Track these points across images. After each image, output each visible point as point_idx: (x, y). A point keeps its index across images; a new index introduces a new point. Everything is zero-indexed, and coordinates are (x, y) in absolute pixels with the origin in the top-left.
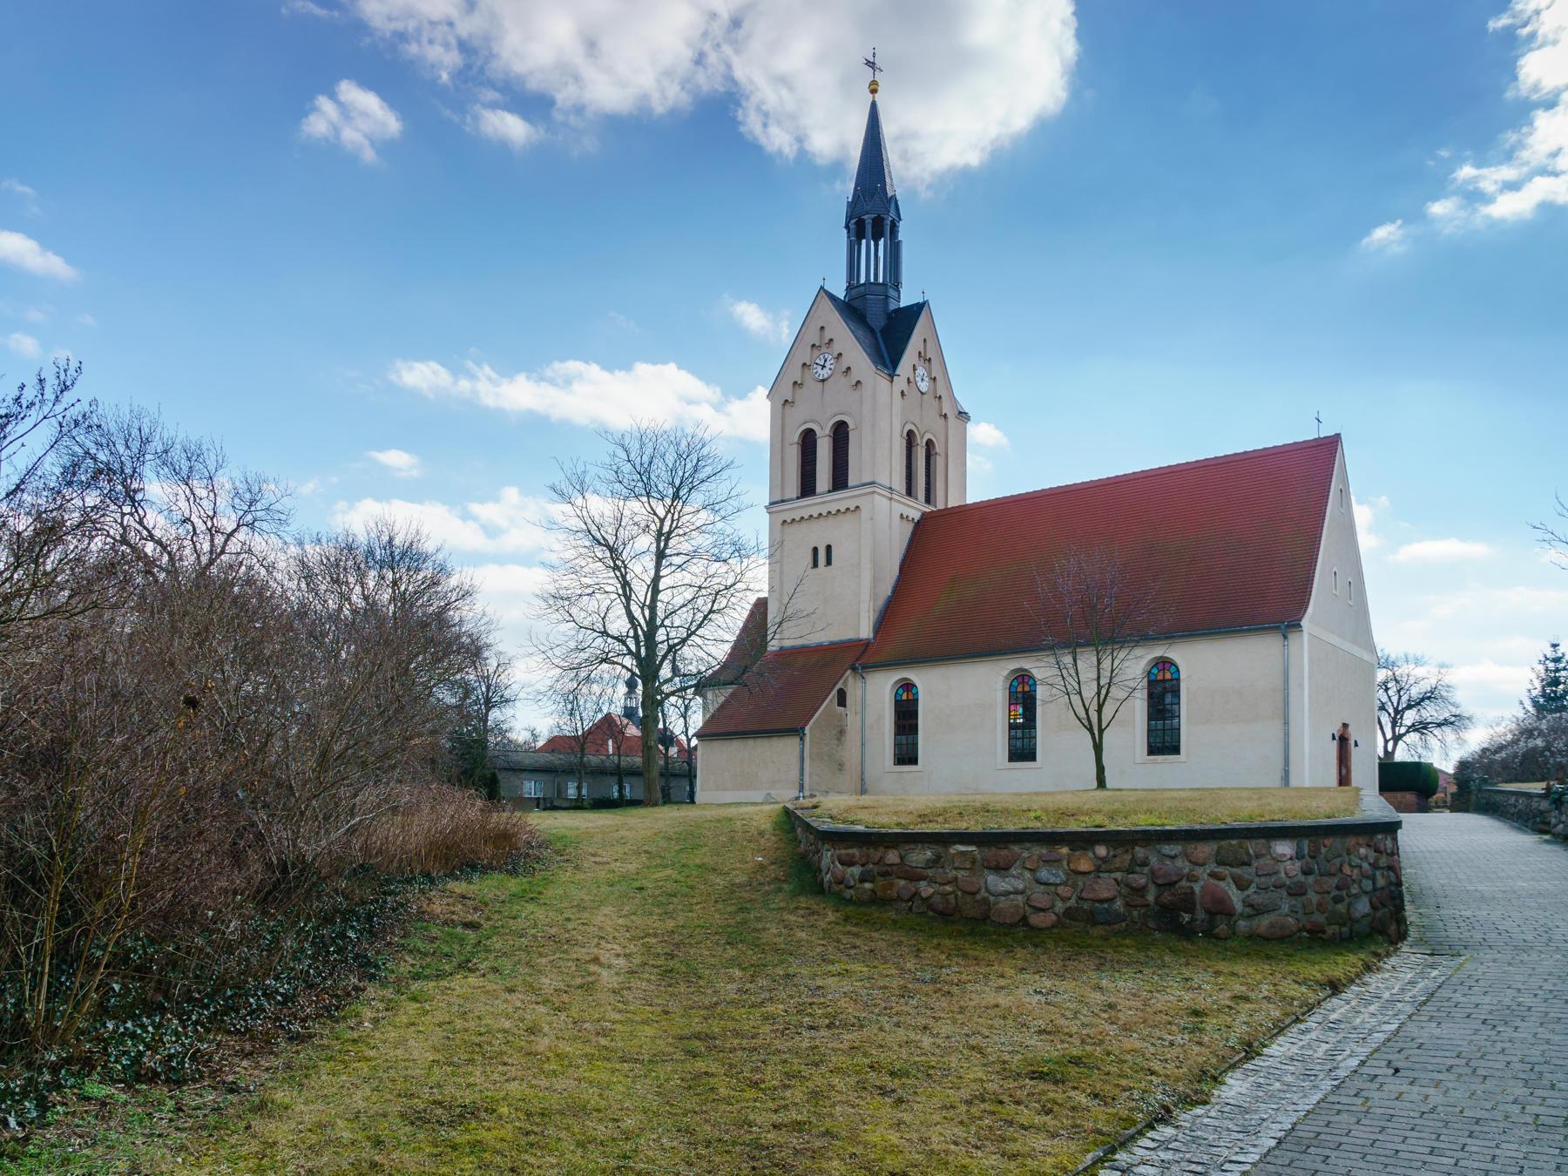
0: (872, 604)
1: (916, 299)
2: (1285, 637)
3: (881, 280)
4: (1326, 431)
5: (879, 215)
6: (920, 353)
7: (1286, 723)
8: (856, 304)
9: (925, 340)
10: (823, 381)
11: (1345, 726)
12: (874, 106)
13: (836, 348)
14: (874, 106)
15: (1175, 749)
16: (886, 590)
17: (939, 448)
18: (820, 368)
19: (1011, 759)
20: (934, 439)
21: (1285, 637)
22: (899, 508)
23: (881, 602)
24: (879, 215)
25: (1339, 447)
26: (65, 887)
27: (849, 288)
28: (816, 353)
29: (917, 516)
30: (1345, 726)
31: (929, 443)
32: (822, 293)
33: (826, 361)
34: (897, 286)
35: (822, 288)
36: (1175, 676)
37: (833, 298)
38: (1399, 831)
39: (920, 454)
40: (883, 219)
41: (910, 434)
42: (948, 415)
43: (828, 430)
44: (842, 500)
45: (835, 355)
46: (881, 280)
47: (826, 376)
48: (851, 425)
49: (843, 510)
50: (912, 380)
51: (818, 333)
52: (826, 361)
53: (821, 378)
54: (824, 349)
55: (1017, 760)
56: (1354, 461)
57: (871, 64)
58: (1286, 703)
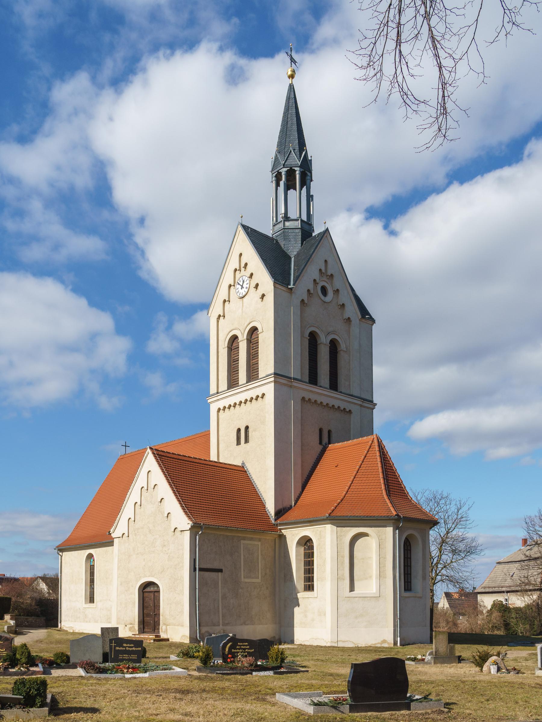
1: (322, 229)
5: (291, 168)
6: (320, 270)
9: (326, 261)
11: (243, 461)
12: (291, 88)
13: (250, 270)
14: (291, 88)
17: (342, 346)
18: (240, 287)
19: (94, 602)
20: (317, 331)
24: (291, 168)
26: (457, 697)
30: (243, 461)
33: (243, 282)
38: (296, 610)
42: (352, 319)
48: (260, 330)
52: (243, 282)
53: (241, 296)
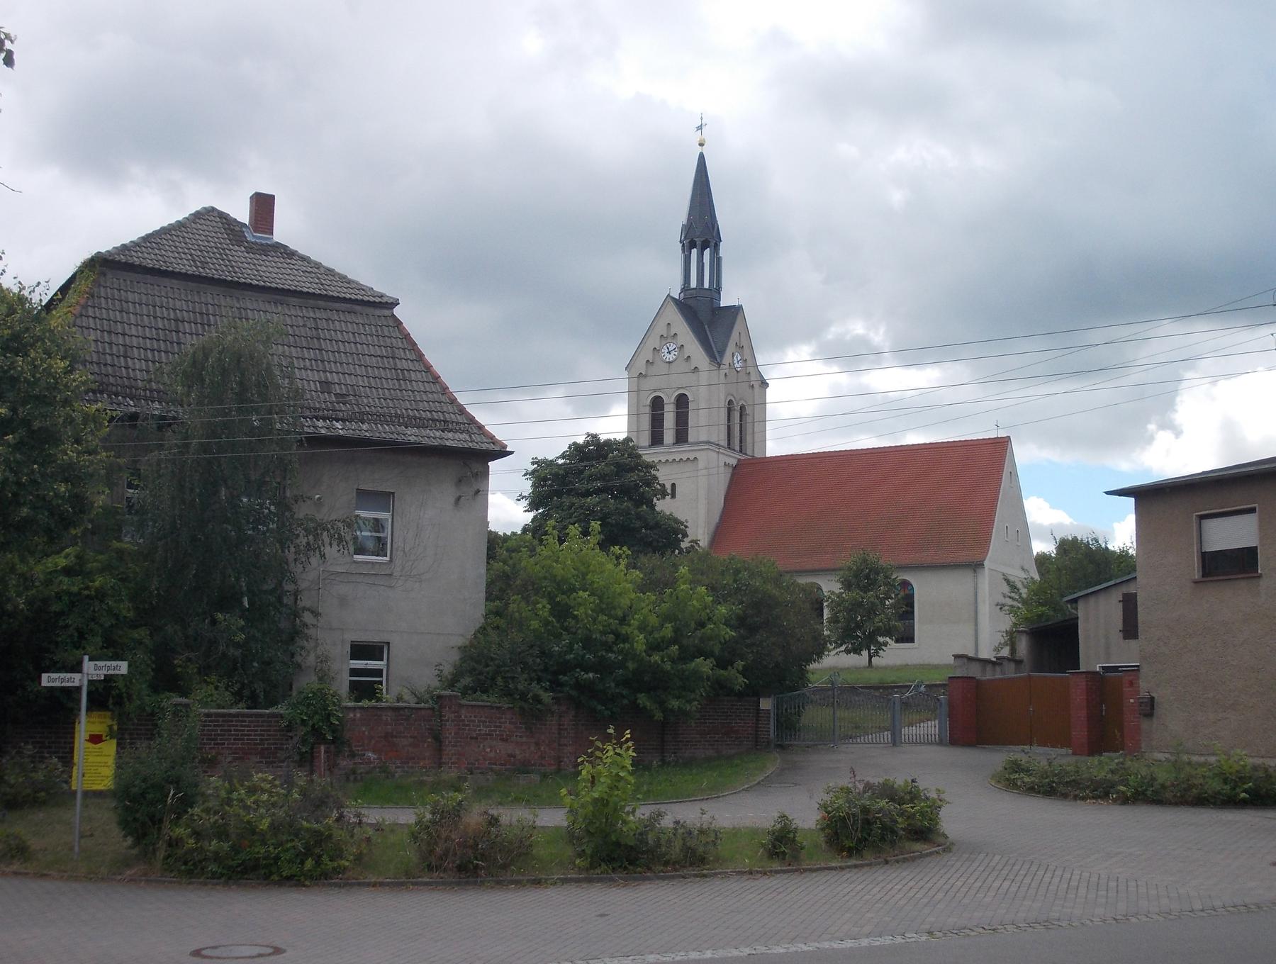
0: (706, 530)
2: (975, 571)
3: (706, 285)
4: (1002, 434)
7: (976, 625)
8: (690, 302)
10: (669, 362)
15: (911, 640)
16: (716, 517)
17: (748, 410)
21: (975, 571)
22: (723, 459)
23: (712, 527)
25: (1009, 446)
27: (683, 290)
28: (664, 342)
29: (733, 462)
31: (742, 408)
32: (669, 299)
34: (718, 290)
35: (668, 295)
36: (911, 592)
37: (674, 299)
39: (737, 415)
40: (709, 242)
41: (730, 402)
43: (673, 399)
44: (683, 452)
45: (679, 346)
46: (706, 285)
47: (671, 360)
49: (685, 459)
50: (731, 364)
51: (666, 328)
54: (669, 340)
55: (1137, 632)
56: (1024, 455)
57: (701, 145)
58: (976, 612)
